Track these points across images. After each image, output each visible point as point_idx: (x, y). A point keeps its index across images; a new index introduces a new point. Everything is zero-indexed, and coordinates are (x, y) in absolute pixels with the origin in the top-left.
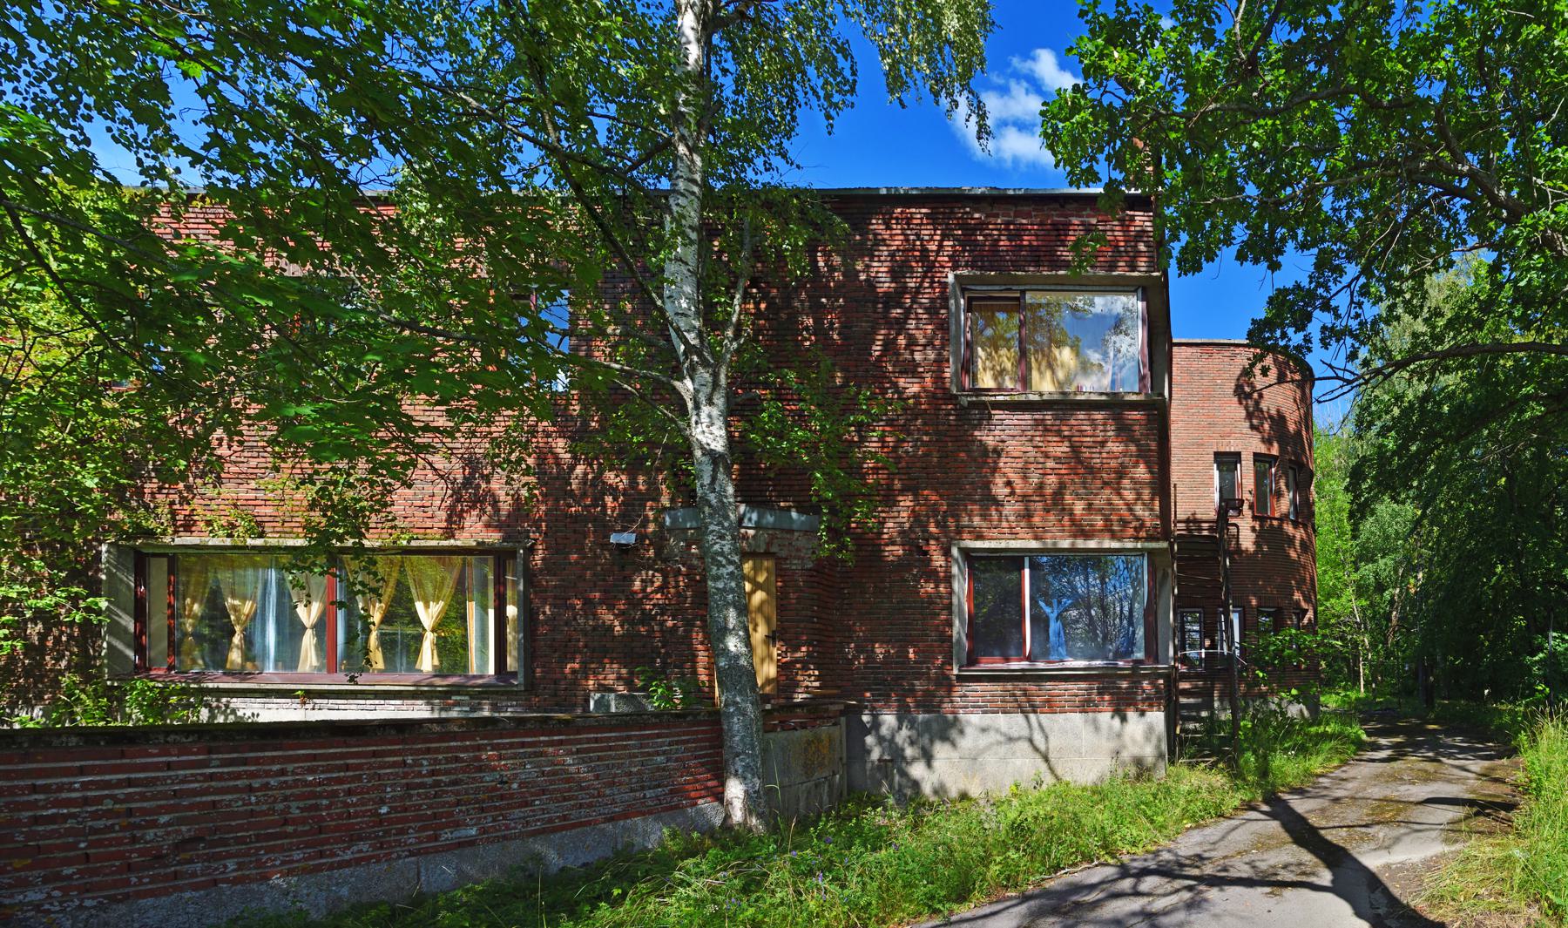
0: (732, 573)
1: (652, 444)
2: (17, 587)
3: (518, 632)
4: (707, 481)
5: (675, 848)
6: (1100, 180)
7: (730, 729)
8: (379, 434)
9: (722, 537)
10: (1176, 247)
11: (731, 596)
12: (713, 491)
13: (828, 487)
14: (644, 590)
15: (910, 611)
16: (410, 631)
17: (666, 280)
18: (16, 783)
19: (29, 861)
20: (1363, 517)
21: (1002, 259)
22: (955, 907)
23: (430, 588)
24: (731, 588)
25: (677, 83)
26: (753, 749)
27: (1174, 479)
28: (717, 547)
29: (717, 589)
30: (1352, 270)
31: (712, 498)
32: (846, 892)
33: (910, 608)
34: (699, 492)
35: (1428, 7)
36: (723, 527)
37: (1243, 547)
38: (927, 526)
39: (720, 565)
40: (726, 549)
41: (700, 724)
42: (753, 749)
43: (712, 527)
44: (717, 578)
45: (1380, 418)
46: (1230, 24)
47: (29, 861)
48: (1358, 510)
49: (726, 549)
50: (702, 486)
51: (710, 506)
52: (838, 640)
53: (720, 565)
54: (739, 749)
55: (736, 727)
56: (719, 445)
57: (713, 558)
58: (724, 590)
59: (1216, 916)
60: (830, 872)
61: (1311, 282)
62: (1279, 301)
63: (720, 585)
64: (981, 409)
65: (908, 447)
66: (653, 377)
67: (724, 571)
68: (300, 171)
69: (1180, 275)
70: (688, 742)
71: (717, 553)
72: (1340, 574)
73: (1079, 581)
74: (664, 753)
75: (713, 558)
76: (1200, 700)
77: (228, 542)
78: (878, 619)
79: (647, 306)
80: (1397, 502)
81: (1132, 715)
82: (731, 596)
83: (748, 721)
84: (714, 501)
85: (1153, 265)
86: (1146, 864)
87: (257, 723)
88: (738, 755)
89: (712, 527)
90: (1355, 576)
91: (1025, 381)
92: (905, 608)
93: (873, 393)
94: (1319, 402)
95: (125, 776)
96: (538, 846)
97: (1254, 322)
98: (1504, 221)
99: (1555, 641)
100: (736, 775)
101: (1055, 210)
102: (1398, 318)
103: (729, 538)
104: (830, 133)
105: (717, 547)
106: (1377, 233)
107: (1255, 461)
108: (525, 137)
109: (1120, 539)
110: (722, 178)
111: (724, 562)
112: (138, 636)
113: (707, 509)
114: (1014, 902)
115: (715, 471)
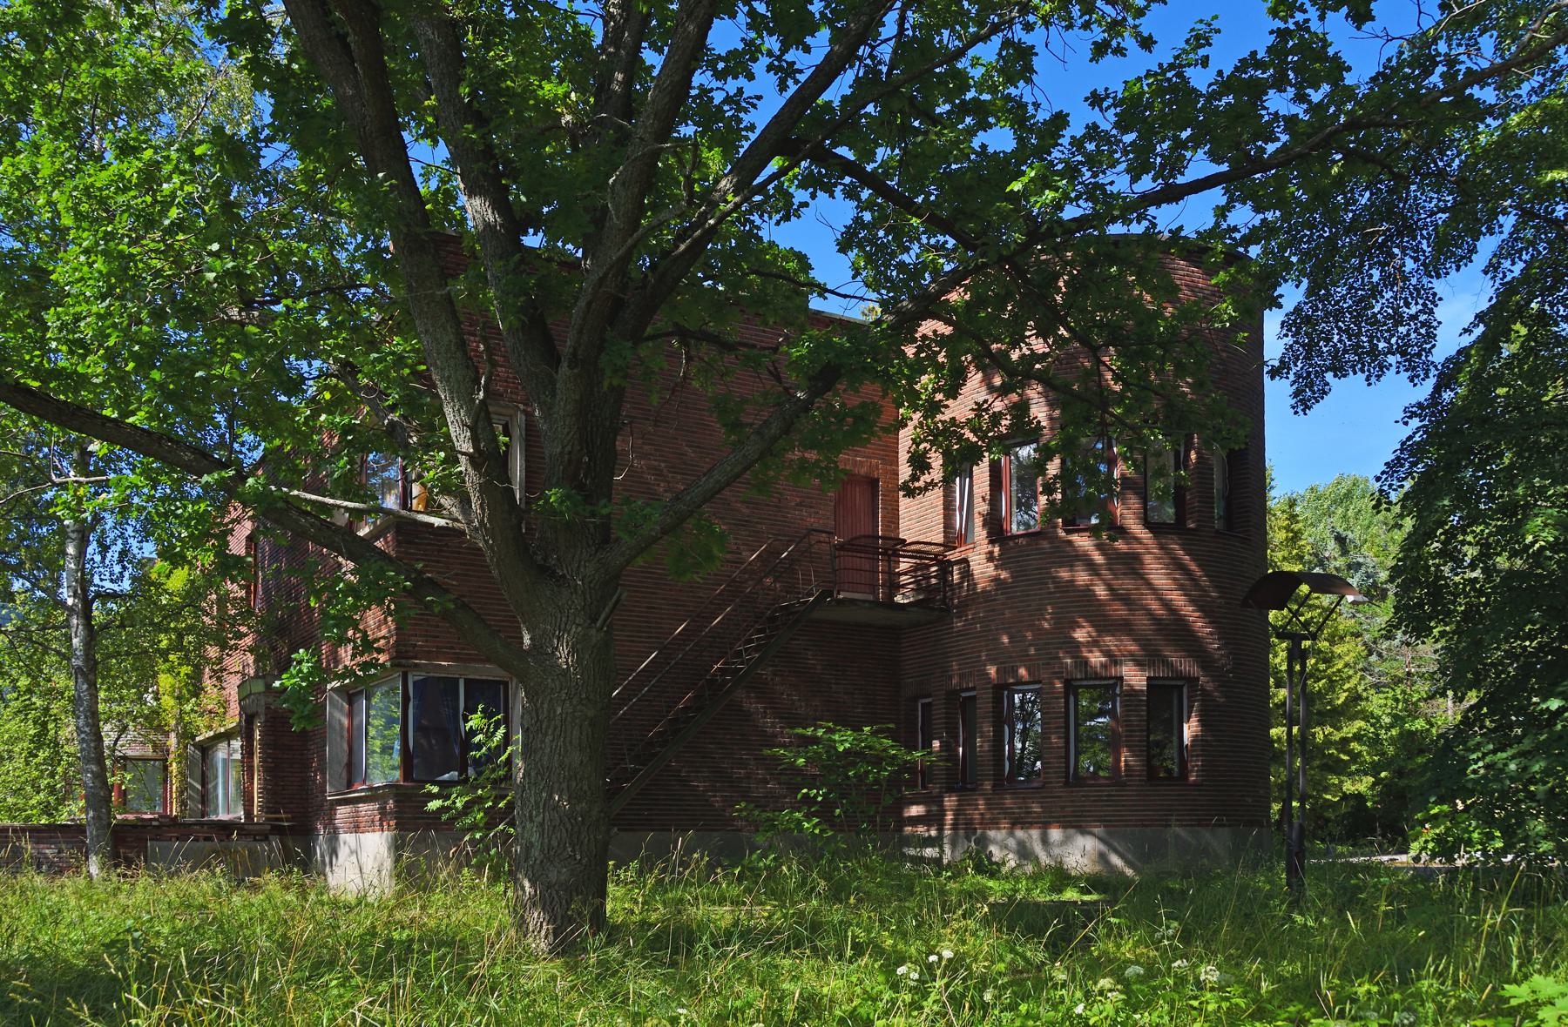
6: (1280, 306)
13: (888, 292)
14: (1374, 769)
17: (398, 767)
18: (338, 502)
19: (1006, 728)
21: (290, 434)
23: (467, 144)
47: (1006, 728)
62: (105, 13)
65: (1457, 136)
77: (212, 733)
81: (844, 230)
94: (911, 493)
98: (1475, 465)
102: (1120, 51)
114: (1072, 699)
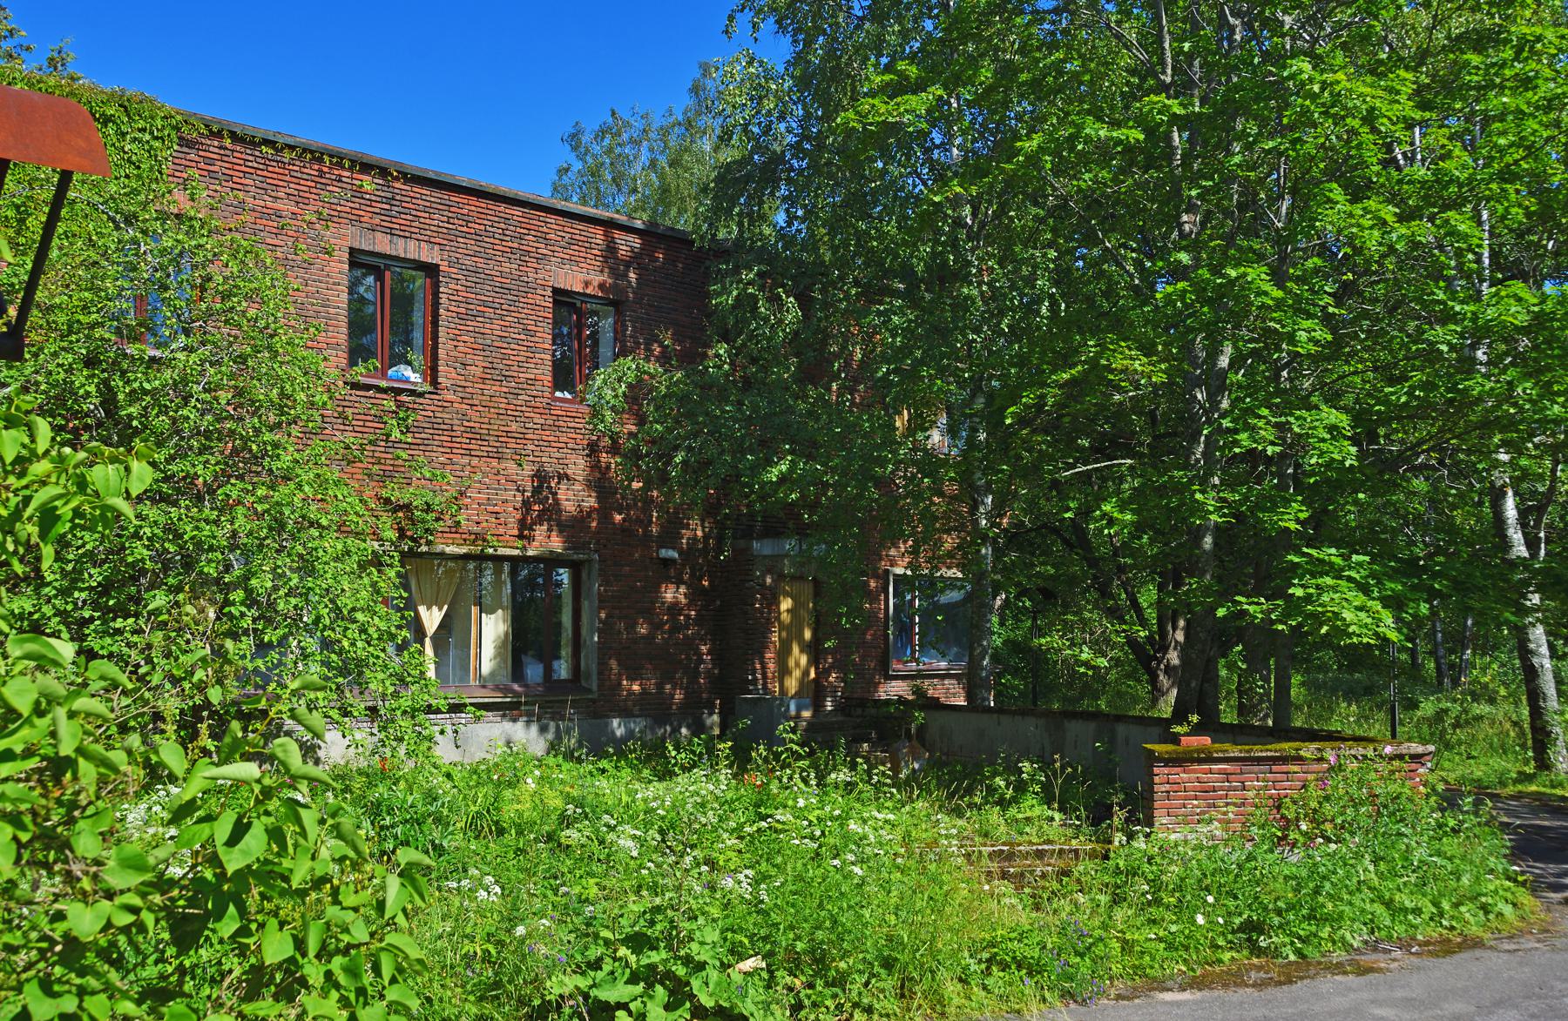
1: (162, 268)
2: (117, 626)
8: (264, 699)
22: (65, 635)
25: (682, 609)
35: (856, 6)
38: (1319, 255)
46: (3, 993)
66: (1533, 793)
68: (614, 664)
73: (645, 217)
79: (1160, 759)
85: (161, 614)
86: (616, 216)
87: (36, 289)
91: (1035, 704)
95: (1543, 545)
96: (229, 146)
99: (5, 513)
106: (1453, 491)
107: (555, 302)
108: (187, 873)
109: (1115, 124)
110: (1264, 372)
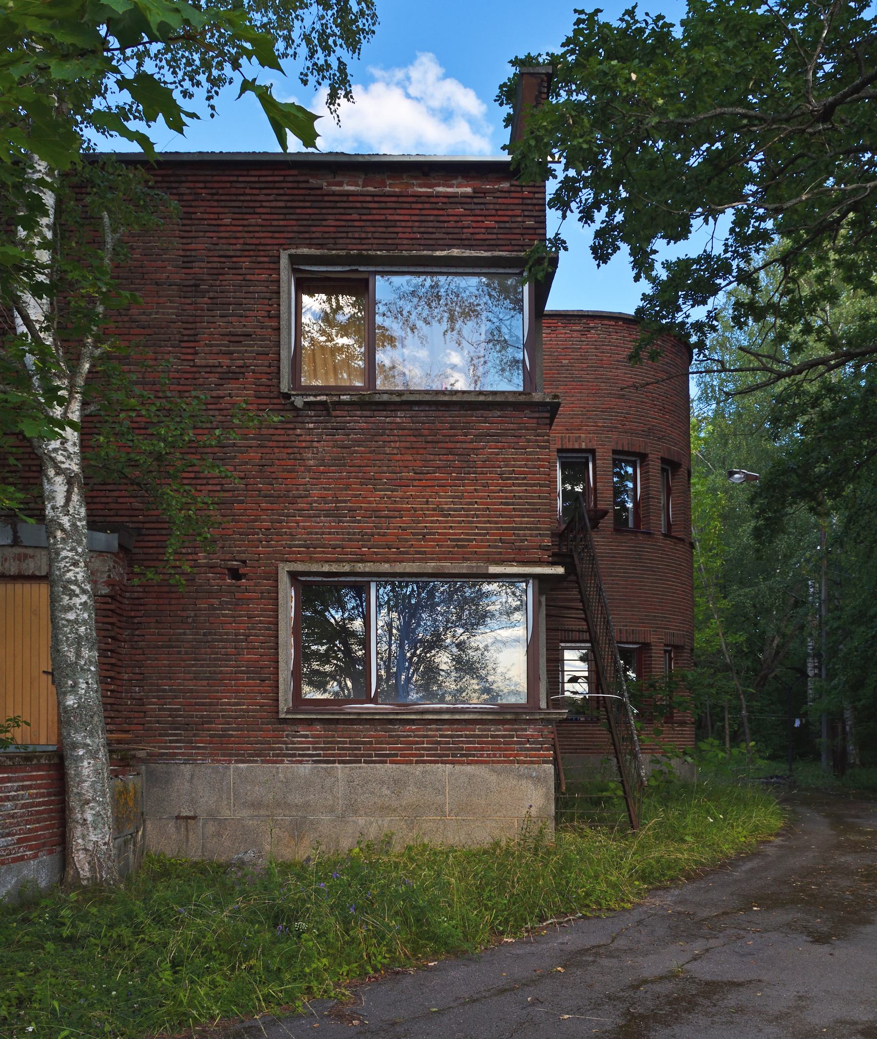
0: (85, 602)
3: (404, 176)
4: (60, 501)
5: (741, 639)
7: (78, 774)
9: (75, 564)
10: (30, 337)
11: (83, 629)
12: (67, 513)
15: (221, 644)
16: (37, 462)
20: (339, 67)
24: (84, 620)
26: (104, 796)
27: (206, 151)
28: (70, 575)
29: (68, 621)
30: (749, 663)
31: (65, 521)
32: (653, 173)
33: (221, 641)
34: (49, 512)
36: (77, 553)
37: (630, 310)
39: (72, 594)
40: (80, 577)
41: (38, 768)
42: (104, 796)
43: (64, 553)
44: (70, 608)
45: (804, 412)
48: (767, 526)
49: (80, 577)
50: (54, 508)
51: (63, 530)
52: (126, 676)
53: (72, 594)
54: (89, 796)
55: (85, 772)
56: (772, 220)
57: (65, 587)
58: (76, 621)
59: (446, 331)
60: (815, 675)
61: (726, 251)
63: (71, 616)
64: (75, 746)
67: (77, 601)
69: (599, 266)
70: (30, 787)
71: (70, 581)
72: (715, 622)
74: (14, 798)
75: (65, 587)
76: (287, 130)
78: (179, 653)
80: (818, 514)
82: (83, 629)
83: (99, 766)
84: (67, 525)
88: (87, 802)
89: (64, 553)
90: (725, 604)
92: (214, 641)
93: (241, 893)
97: (525, 63)
100: (41, 438)
101: (416, 178)
103: (82, 564)
104: (212, 116)
105: (70, 575)
111: (78, 591)
112: (589, 631)
113: (59, 534)
115: (69, 492)
